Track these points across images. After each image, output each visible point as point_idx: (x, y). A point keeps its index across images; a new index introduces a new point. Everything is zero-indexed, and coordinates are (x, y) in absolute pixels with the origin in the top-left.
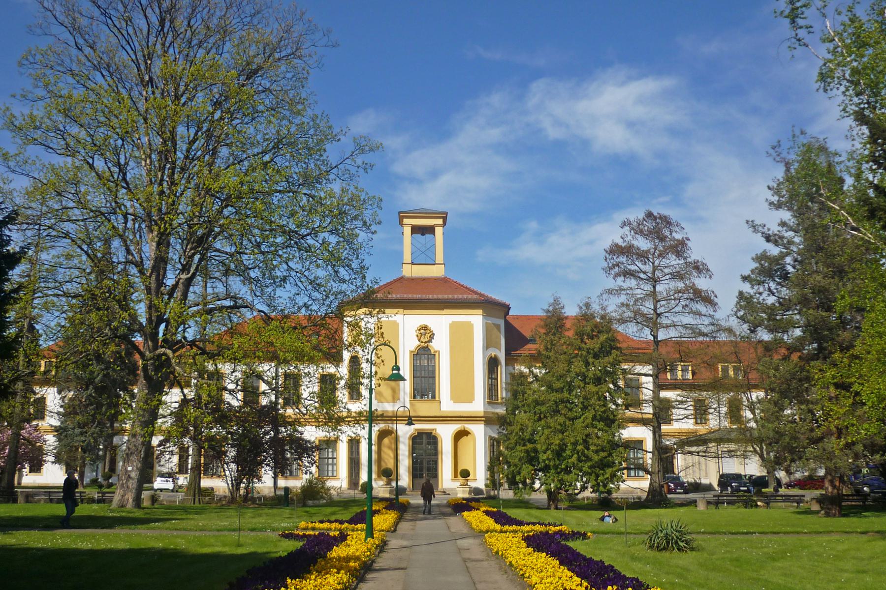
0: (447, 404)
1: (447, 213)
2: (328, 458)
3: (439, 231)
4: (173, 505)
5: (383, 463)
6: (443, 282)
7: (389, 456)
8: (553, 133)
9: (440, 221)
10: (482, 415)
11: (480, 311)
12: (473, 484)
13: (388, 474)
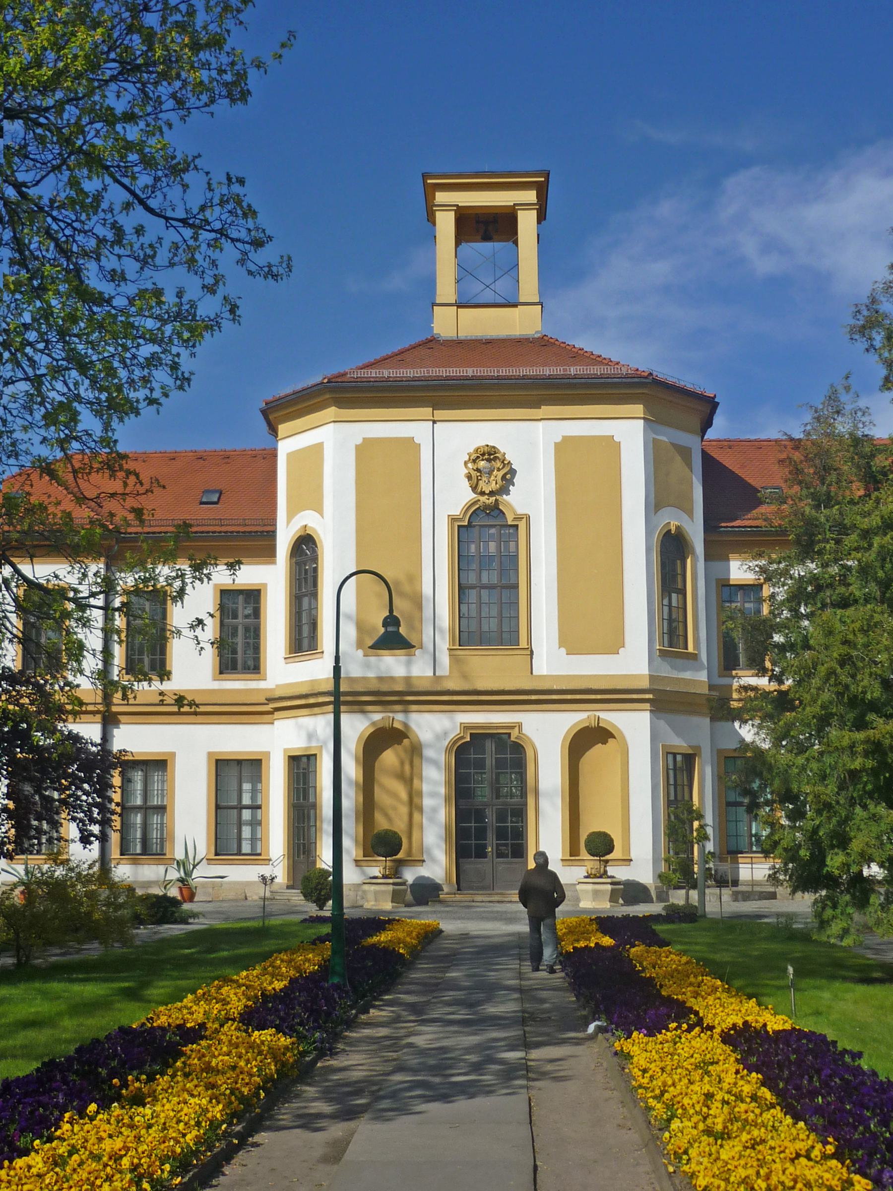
0: (550, 658)
1: (547, 175)
2: (241, 808)
3: (527, 222)
4: (788, 927)
5: (379, 817)
6: (542, 345)
7: (395, 796)
8: (766, 266)
9: (531, 196)
10: (645, 684)
11: (638, 409)
12: (620, 873)
13: (385, 845)
